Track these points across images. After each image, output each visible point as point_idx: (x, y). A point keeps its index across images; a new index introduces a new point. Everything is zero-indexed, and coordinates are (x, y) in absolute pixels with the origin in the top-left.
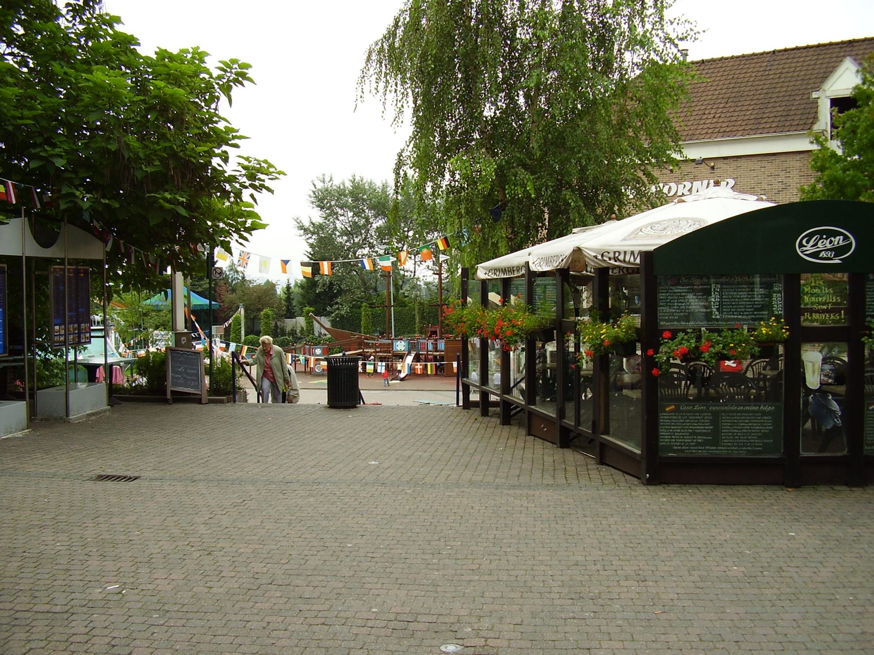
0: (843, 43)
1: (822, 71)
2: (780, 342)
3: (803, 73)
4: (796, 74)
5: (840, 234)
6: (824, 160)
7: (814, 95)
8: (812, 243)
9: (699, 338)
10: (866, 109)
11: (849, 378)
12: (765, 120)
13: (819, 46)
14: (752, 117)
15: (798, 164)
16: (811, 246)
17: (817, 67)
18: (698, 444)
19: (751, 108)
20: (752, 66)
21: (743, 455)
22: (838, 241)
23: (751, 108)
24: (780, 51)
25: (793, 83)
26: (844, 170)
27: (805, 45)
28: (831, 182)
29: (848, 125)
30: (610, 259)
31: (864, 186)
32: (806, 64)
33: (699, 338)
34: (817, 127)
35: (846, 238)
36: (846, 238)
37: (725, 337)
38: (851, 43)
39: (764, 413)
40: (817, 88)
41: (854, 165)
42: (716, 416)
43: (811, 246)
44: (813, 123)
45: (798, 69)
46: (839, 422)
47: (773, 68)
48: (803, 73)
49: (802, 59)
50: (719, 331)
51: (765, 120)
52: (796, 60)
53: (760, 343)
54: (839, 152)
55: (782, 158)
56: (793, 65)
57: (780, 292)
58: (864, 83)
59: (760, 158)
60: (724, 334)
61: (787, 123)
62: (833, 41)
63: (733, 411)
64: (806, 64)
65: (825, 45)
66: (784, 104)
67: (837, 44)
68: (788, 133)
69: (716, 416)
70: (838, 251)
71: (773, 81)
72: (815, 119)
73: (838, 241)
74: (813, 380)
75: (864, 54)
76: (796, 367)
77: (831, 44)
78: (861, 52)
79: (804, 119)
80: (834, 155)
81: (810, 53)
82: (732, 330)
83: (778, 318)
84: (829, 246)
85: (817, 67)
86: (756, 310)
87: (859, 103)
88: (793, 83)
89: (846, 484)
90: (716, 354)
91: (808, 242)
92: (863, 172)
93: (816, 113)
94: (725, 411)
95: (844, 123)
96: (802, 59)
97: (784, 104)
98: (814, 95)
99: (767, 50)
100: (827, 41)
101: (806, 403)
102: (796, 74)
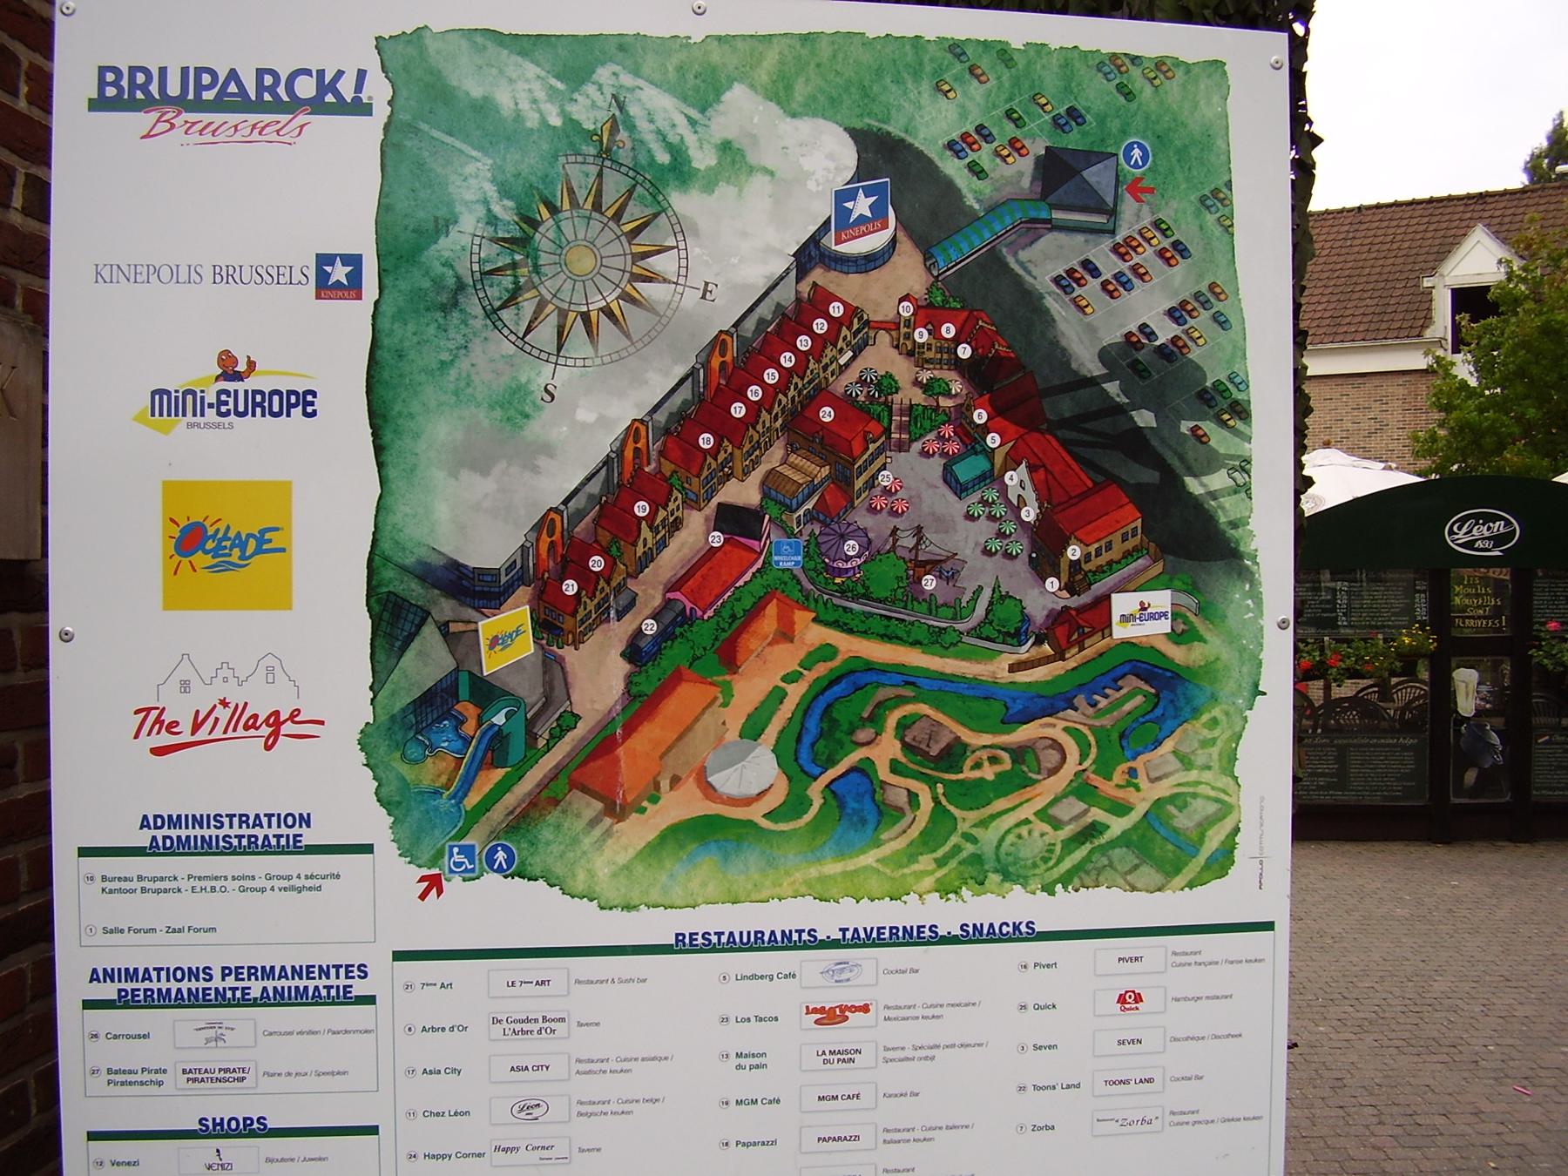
0: (1469, 197)
1: (1437, 241)
2: (1424, 656)
3: (1406, 245)
4: (1395, 246)
5: (1502, 518)
6: (1450, 396)
7: (1427, 283)
8: (1465, 529)
9: (1322, 649)
10: (1514, 320)
11: (1510, 705)
12: (1348, 320)
13: (1431, 201)
14: (1328, 314)
15: (1401, 391)
16: (1465, 534)
17: (1429, 235)
18: (1320, 788)
19: (1325, 299)
20: (1325, 230)
21: (1377, 800)
22: (1498, 527)
23: (1325, 299)
24: (1369, 208)
25: (1391, 261)
26: (1481, 410)
27: (1410, 198)
28: (1461, 429)
29: (1484, 342)
30: (738, 523)
31: (1510, 435)
32: (1411, 229)
33: (1322, 649)
34: (1429, 334)
35: (1508, 523)
36: (1508, 523)
37: (1357, 649)
38: (1482, 197)
39: (1405, 748)
40: (1432, 271)
41: (1493, 403)
42: (1342, 750)
43: (1465, 534)
44: (1424, 327)
45: (1399, 238)
46: (1500, 759)
47: (1358, 235)
48: (1406, 245)
49: (1404, 222)
50: (1348, 641)
51: (1348, 320)
52: (1395, 223)
53: (1400, 656)
54: (1473, 382)
55: (1376, 381)
56: (1391, 231)
57: (1424, 592)
58: (1509, 280)
59: (1340, 381)
60: (1354, 645)
61: (1384, 326)
62: (1454, 193)
63: (1362, 745)
64: (1411, 229)
65: (1440, 200)
66: (1377, 294)
67: (1460, 198)
68: (1384, 342)
69: (1342, 756)
70: (1498, 540)
71: (1359, 257)
72: (1428, 320)
73: (1498, 527)
74: (1466, 705)
75: (1503, 216)
76: (1443, 690)
77: (1450, 198)
78: (1498, 213)
79: (1408, 322)
80: (1464, 385)
81: (1418, 213)
82: (1365, 640)
83: (1423, 625)
84: (1487, 534)
85: (1429, 235)
86: (1394, 614)
87: (1502, 309)
88: (1391, 261)
89: (1510, 840)
90: (1347, 669)
91: (1460, 528)
92: (1507, 414)
93: (1429, 309)
94: (1355, 746)
95: (1479, 338)
96: (1404, 222)
97: (1377, 294)
98: (1427, 283)
99: (1348, 206)
100: (1445, 194)
101: (1457, 732)
102: (1395, 246)
